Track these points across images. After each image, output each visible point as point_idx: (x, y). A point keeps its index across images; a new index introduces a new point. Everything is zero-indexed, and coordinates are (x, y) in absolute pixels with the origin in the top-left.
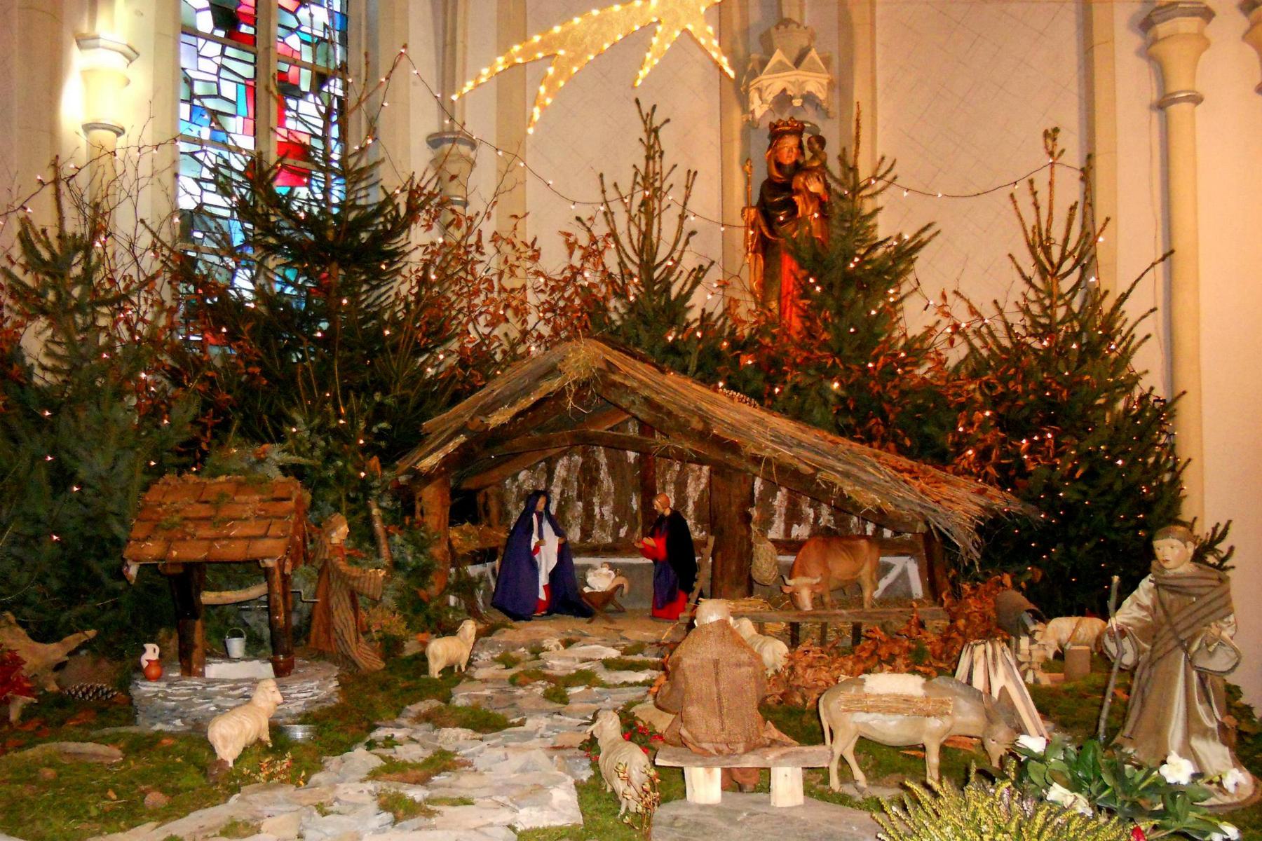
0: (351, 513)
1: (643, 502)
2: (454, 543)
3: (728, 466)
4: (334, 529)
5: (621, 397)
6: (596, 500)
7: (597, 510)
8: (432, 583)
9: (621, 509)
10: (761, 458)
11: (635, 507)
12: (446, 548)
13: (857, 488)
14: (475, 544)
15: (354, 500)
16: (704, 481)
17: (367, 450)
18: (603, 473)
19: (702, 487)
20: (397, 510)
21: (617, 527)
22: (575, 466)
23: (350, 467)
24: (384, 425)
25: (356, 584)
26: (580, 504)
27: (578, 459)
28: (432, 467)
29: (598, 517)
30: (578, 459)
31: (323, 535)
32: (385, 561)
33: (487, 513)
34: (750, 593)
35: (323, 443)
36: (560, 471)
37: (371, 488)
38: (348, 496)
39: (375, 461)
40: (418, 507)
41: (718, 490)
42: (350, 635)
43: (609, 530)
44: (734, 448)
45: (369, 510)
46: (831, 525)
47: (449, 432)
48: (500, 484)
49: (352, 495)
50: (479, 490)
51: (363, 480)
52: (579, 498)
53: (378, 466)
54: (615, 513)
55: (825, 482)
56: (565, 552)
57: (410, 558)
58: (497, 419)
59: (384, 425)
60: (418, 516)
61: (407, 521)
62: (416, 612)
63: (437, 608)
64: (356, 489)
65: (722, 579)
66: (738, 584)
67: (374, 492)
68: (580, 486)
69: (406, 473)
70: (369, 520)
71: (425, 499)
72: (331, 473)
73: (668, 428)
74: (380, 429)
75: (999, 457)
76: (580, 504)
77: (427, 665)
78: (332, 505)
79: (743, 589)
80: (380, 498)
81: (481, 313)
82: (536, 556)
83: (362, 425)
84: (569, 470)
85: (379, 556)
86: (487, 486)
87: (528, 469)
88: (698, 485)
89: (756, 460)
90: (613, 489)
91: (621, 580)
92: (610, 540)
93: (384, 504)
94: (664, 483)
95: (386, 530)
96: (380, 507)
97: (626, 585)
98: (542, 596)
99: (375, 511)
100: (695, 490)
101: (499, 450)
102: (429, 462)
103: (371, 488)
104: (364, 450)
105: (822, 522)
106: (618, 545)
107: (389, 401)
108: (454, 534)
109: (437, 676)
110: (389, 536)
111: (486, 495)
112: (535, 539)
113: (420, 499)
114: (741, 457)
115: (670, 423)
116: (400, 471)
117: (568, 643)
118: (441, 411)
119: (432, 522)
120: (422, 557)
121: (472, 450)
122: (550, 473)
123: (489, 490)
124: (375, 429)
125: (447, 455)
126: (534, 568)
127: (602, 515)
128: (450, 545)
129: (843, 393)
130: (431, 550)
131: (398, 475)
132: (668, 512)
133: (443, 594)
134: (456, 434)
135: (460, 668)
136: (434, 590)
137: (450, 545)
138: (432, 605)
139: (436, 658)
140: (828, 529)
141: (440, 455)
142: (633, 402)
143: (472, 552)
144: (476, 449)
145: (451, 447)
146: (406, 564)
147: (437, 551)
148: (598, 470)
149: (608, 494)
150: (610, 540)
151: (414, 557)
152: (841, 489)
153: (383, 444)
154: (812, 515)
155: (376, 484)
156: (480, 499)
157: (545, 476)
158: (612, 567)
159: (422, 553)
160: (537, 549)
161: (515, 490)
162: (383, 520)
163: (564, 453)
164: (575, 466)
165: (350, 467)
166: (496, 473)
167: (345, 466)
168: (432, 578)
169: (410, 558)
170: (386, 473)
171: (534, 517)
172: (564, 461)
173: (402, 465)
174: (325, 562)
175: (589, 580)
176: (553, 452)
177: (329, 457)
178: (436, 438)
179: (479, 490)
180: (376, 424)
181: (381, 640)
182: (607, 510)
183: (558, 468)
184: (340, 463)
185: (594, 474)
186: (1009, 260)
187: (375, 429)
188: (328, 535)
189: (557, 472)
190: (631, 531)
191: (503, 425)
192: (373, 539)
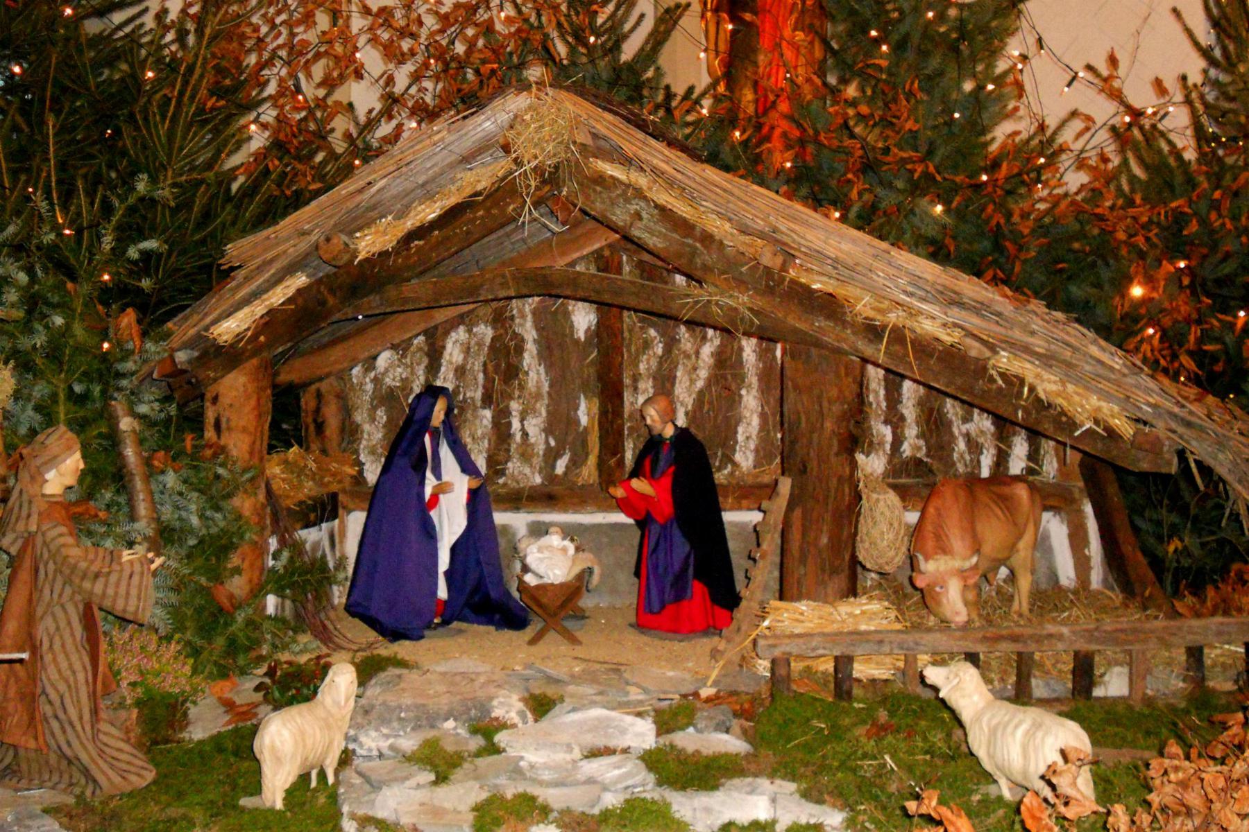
0: (79, 426)
1: (603, 413)
2: (275, 487)
3: (818, 344)
4: (53, 461)
5: (613, 203)
6: (515, 406)
7: (516, 424)
8: (237, 571)
9: (561, 422)
10: (884, 327)
11: (584, 420)
12: (262, 497)
13: (1070, 388)
14: (309, 489)
15: (82, 399)
16: (703, 374)
17: (119, 295)
18: (530, 358)
19: (700, 384)
20: (169, 419)
21: (552, 456)
22: (480, 345)
23: (78, 330)
24: (150, 244)
25: (98, 588)
26: (487, 414)
27: (486, 332)
28: (239, 337)
29: (518, 437)
30: (486, 332)
31: (24, 475)
32: (143, 526)
33: (320, 427)
34: (852, 591)
35: (23, 278)
36: (453, 353)
37: (120, 375)
38: (70, 388)
39: (128, 319)
40: (210, 415)
41: (796, 387)
42: (78, 708)
43: (537, 461)
44: (829, 306)
45: (113, 421)
46: (921, 454)
47: (277, 265)
48: (343, 375)
49: (78, 388)
50: (305, 385)
51: (104, 357)
52: (487, 400)
53: (135, 330)
54: (548, 430)
55: (1002, 375)
56: (478, 503)
57: (195, 521)
58: (368, 244)
59: (150, 244)
60: (210, 434)
61: (189, 443)
62: (207, 631)
63: (250, 623)
64: (86, 376)
65: (803, 560)
66: (834, 571)
67: (124, 383)
68: (489, 381)
69: (188, 345)
70: (113, 440)
71: (225, 400)
72: (40, 340)
73: (706, 268)
74: (142, 252)
75: (1200, 341)
76: (487, 414)
77: (258, 771)
78: (38, 409)
79: (841, 581)
80: (134, 396)
81: (318, 56)
82: (433, 514)
83: (108, 242)
84: (467, 351)
85: (133, 518)
86: (320, 379)
87: (394, 347)
88: (692, 382)
89: (873, 331)
90: (546, 387)
91: (587, 560)
92: (538, 480)
93: (143, 409)
94: (636, 379)
95: (148, 462)
96: (133, 414)
97: (597, 570)
98: (442, 593)
99: (126, 424)
100: (689, 389)
101: (373, 302)
102: (230, 328)
103: (120, 375)
104: (107, 295)
105: (907, 450)
106: (557, 489)
107: (165, 193)
108: (275, 469)
109: (279, 805)
110: (151, 472)
111: (319, 395)
112: (430, 482)
113: (215, 400)
114: (844, 324)
115: (707, 257)
116: (175, 341)
117: (540, 706)
118: (244, 232)
119: (238, 445)
120: (218, 516)
121: (323, 303)
122: (435, 356)
123: (324, 386)
124: (133, 253)
125: (271, 312)
126: (429, 533)
127: (525, 434)
128: (269, 493)
129: (948, 220)
130: (236, 501)
131: (173, 350)
132: (669, 432)
133: (258, 592)
134: (290, 270)
135: (322, 775)
136: (237, 586)
137: (269, 493)
138: (240, 617)
139: (278, 760)
140: (919, 462)
141: (258, 309)
142: (638, 216)
143: (301, 503)
144: (331, 301)
145: (278, 296)
146: (186, 530)
147: (245, 504)
148: (520, 350)
149: (538, 396)
150: (538, 480)
151: (202, 516)
152: (1032, 389)
153: (146, 283)
154: (889, 438)
155: (130, 365)
156: (307, 401)
157: (426, 361)
158: (569, 532)
159: (218, 509)
160: (435, 499)
161: (369, 387)
162: (141, 442)
163: (460, 320)
164: (480, 345)
165: (78, 330)
166: (336, 353)
167: (68, 326)
168: (234, 560)
169: (195, 521)
170: (149, 346)
171: (427, 439)
172: (460, 334)
173: (183, 329)
174: (29, 540)
175: (531, 560)
176: (441, 316)
177: (34, 304)
178: (247, 279)
179: (305, 385)
180: (135, 242)
181: (139, 703)
182: (534, 427)
183: (449, 346)
184: (59, 321)
185: (514, 360)
186: (1172, 19)
187: (133, 253)
188: (38, 477)
189: (446, 355)
190: (575, 463)
191: (384, 254)
192: (120, 478)
